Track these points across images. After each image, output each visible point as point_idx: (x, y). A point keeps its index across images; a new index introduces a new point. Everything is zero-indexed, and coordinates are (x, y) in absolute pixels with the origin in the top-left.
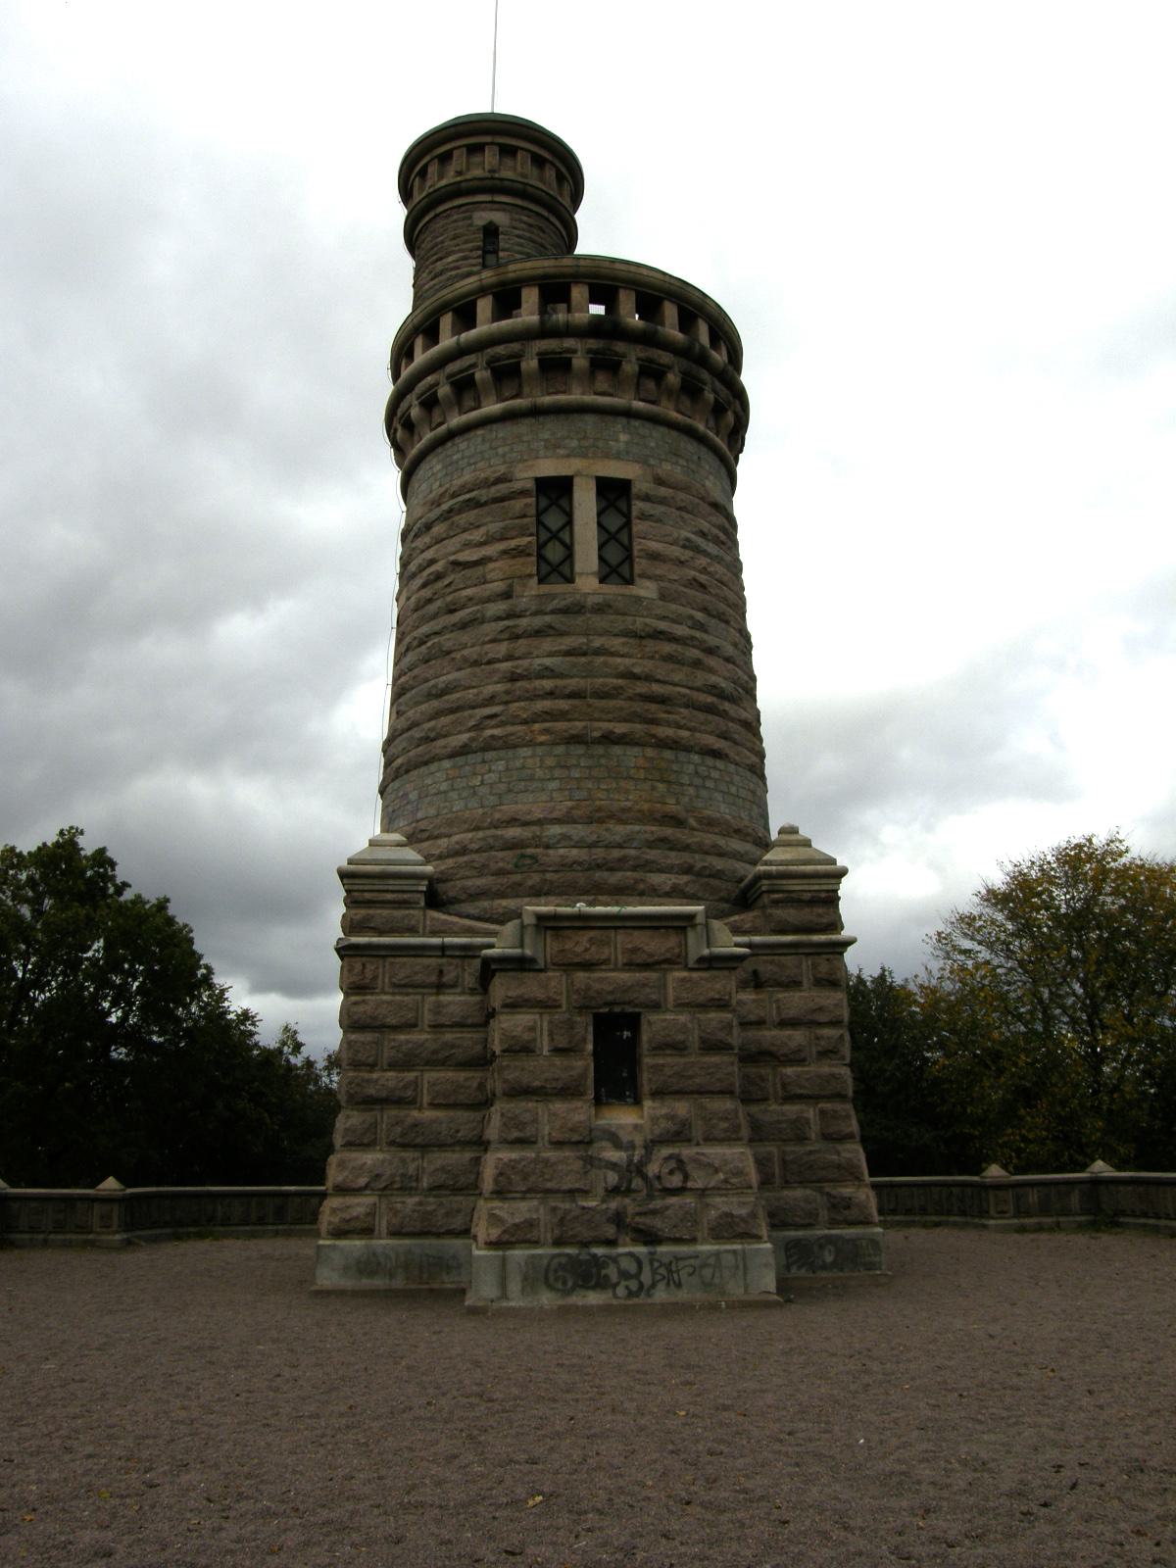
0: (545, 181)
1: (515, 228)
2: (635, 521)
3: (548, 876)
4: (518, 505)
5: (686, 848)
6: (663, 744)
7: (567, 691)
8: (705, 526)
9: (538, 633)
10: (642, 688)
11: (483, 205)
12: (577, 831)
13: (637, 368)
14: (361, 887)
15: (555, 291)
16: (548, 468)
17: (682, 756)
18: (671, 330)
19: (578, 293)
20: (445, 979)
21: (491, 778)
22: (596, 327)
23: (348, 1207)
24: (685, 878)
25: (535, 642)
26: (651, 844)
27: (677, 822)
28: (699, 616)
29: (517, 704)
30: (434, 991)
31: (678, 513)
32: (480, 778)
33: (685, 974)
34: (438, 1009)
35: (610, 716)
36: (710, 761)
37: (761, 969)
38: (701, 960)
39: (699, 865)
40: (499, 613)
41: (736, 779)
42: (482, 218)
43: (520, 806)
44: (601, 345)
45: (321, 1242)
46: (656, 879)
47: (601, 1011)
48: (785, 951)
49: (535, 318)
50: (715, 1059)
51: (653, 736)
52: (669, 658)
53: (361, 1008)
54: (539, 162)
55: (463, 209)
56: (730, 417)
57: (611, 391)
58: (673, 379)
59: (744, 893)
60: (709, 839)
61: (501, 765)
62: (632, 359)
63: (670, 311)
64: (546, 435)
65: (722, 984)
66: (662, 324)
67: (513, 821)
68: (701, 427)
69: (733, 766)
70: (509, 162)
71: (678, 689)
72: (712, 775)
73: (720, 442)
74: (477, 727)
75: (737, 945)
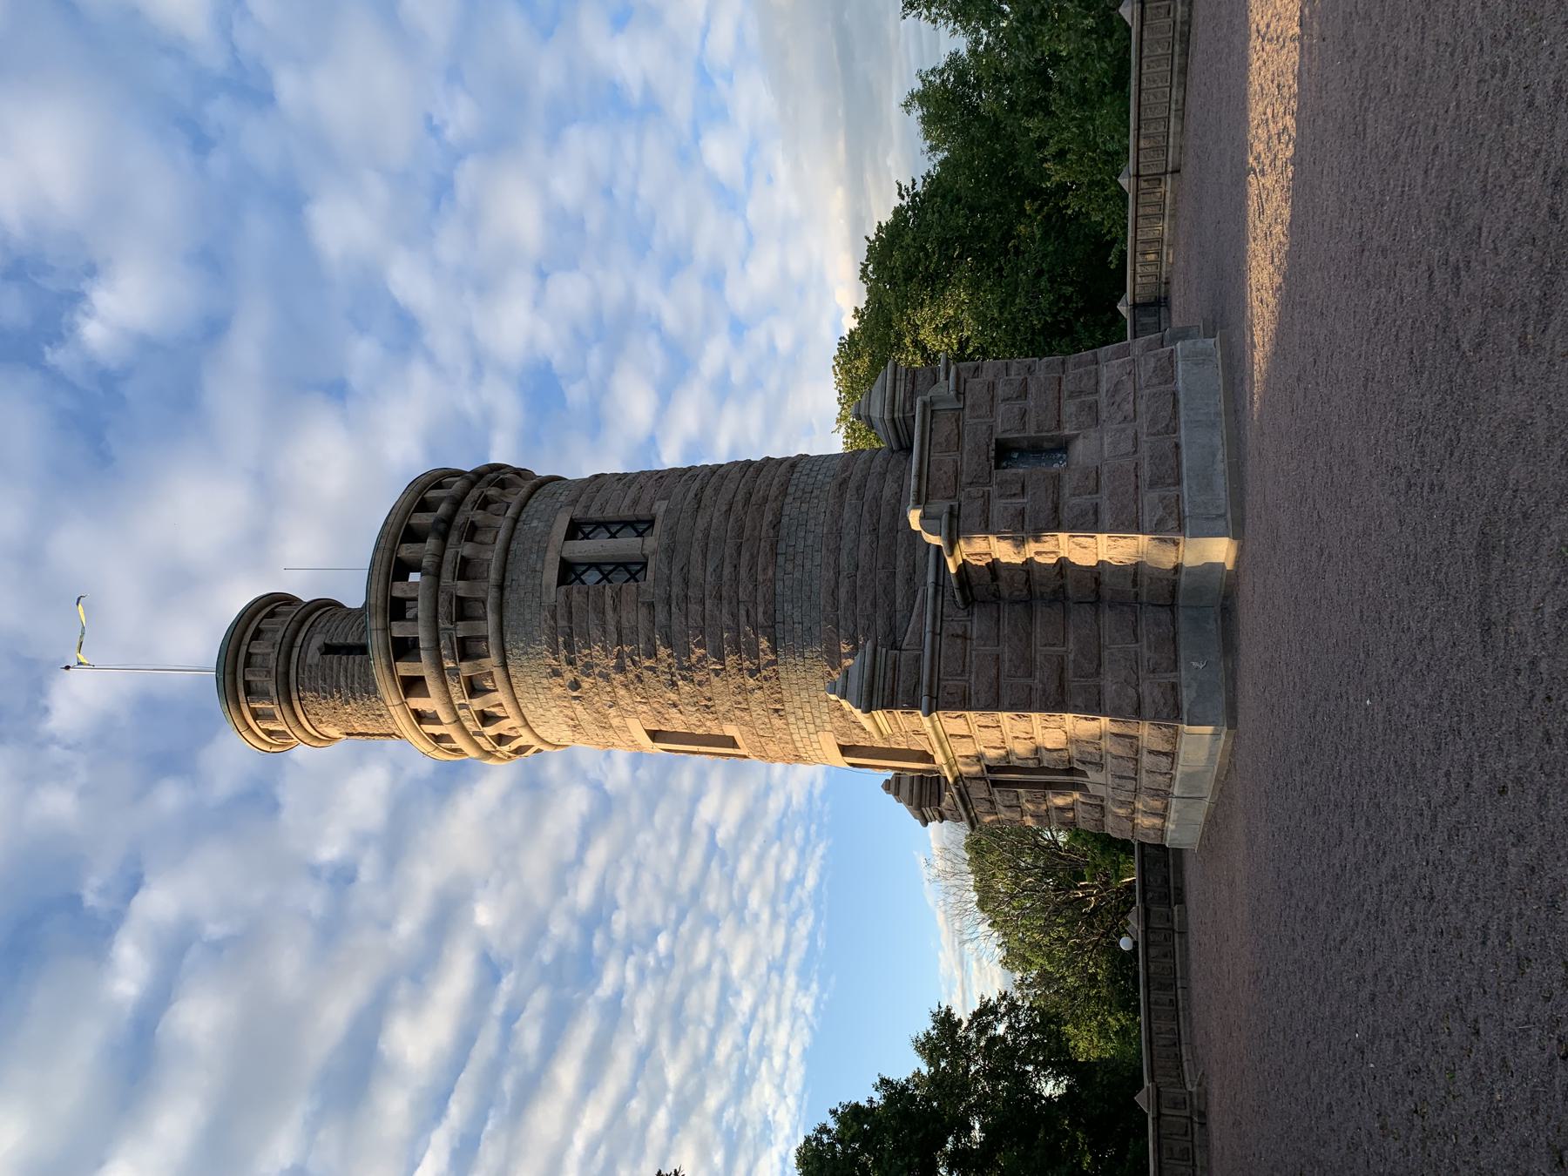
0: (278, 628)
3: (880, 565)
5: (865, 478)
9: (686, 582)
10: (738, 506)
11: (302, 655)
12: (847, 544)
14: (880, 698)
16: (551, 574)
19: (399, 590)
21: (797, 616)
26: (861, 498)
27: (843, 484)
29: (740, 595)
32: (796, 626)
33: (967, 411)
35: (758, 525)
39: (878, 469)
40: (665, 613)
42: (313, 656)
46: (887, 492)
50: (1033, 389)
51: (776, 497)
52: (717, 491)
54: (258, 634)
55: (300, 671)
57: (494, 532)
62: (468, 513)
63: (407, 551)
64: (523, 578)
67: (834, 593)
73: (514, 499)
75: (947, 378)
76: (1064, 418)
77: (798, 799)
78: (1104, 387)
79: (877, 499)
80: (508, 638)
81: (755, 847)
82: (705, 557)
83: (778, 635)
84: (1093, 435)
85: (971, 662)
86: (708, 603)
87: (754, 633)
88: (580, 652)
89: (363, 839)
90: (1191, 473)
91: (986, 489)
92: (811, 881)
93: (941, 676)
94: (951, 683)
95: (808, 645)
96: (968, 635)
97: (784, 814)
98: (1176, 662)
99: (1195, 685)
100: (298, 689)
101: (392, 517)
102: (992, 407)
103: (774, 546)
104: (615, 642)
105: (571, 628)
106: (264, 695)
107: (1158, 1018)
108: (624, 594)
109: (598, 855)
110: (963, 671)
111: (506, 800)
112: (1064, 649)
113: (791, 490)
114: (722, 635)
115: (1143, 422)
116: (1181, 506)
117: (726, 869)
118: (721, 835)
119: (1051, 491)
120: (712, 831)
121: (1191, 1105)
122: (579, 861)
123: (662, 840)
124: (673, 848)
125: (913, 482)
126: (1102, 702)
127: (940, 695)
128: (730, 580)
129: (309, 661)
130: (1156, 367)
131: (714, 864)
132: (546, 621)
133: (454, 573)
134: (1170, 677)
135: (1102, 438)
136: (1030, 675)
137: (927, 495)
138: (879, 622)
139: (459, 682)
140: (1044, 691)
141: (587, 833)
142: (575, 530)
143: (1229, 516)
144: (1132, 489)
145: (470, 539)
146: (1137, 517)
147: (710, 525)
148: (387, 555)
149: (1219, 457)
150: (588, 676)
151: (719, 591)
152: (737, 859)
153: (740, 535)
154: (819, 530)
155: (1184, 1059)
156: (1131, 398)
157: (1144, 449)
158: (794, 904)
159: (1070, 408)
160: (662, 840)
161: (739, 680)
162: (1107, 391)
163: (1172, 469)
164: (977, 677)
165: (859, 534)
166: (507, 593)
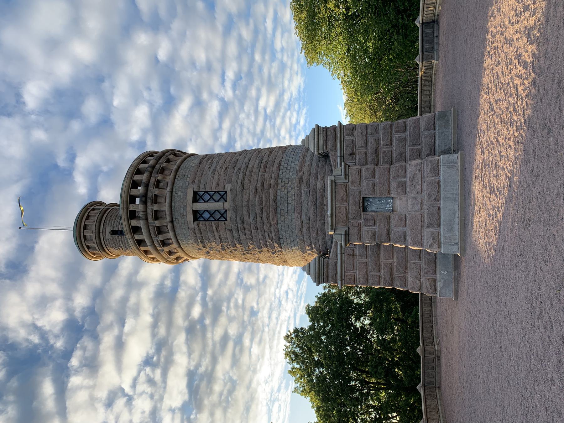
1: (111, 225)
2: (206, 190)
3: (318, 220)
4: (202, 227)
5: (309, 176)
6: (277, 184)
7: (261, 213)
8: (207, 167)
9: (243, 222)
10: (259, 189)
11: (104, 235)
12: (304, 210)
13: (157, 189)
14: (323, 279)
15: (133, 215)
16: (190, 217)
17: (280, 176)
18: (144, 177)
19: (132, 207)
20: (352, 254)
21: (288, 237)
22: (144, 202)
23: (427, 287)
24: (319, 176)
25: (245, 223)
26: (308, 188)
27: (301, 178)
28: (236, 170)
29: (265, 228)
30: (355, 256)
31: (203, 176)
33: (350, 183)
34: (361, 256)
36: (281, 167)
37: (348, 153)
38: (346, 178)
39: (315, 172)
41: (287, 158)
42: (108, 236)
43: (297, 228)
44: (150, 201)
45: (438, 296)
46: (319, 186)
47: (362, 210)
48: (342, 145)
49: (141, 221)
50: (378, 174)
51: (274, 186)
53: (361, 280)
55: (105, 241)
56: (171, 157)
57: (164, 197)
58: (160, 177)
59: (324, 156)
60: (306, 168)
61: (284, 233)
62: (153, 191)
65: (353, 169)
66: (142, 180)
67: (301, 230)
68: (175, 167)
69: (283, 159)
70: (89, 227)
71: (259, 177)
72: (286, 166)
73: (180, 159)
74: (272, 240)
75: (341, 166)
76: (391, 188)
77: (295, 93)
78: (408, 176)
79: (315, 189)
80: (179, 238)
81: (281, 114)
82: (249, 213)
83: (281, 243)
84: (403, 198)
85: (356, 265)
86: (252, 231)
87: (272, 242)
88: (207, 244)
89: (145, 131)
90: (445, 223)
91: (359, 221)
92: (302, 122)
93: (345, 270)
94: (349, 273)
95: (293, 246)
96: (355, 254)
97: (290, 100)
98: (435, 271)
99: (442, 281)
100: (106, 247)
101: (123, 193)
102: (360, 182)
103: (275, 210)
104: (220, 242)
105: (202, 237)
106: (95, 249)
107: (425, 306)
108: (220, 226)
109: (226, 124)
110: (353, 269)
111: (191, 109)
112: (393, 261)
113: (280, 181)
114: (260, 242)
115: (425, 194)
116: (440, 237)
117: (272, 123)
118: (268, 111)
119: (386, 225)
120: (265, 110)
121: (435, 354)
122: (220, 128)
123: (248, 116)
124: (253, 119)
125: (329, 219)
126: (407, 284)
127: (345, 278)
128: (260, 223)
129: (107, 238)
130: (431, 169)
131: (268, 122)
132: (192, 234)
133: (153, 218)
134: (433, 276)
135: (407, 201)
136: (380, 271)
137: (335, 224)
138: (320, 240)
139: (165, 253)
140: (385, 279)
141: (221, 115)
142: (196, 197)
143: (459, 244)
144: (420, 228)
145: (156, 202)
146: (422, 240)
147: (249, 199)
148: (125, 211)
149: (457, 215)
150: (212, 250)
151: (256, 227)
152: (275, 119)
153: (262, 204)
154: (293, 203)
155: (434, 323)
156: (420, 183)
157: (425, 208)
158: (297, 132)
159: (394, 184)
160: (248, 116)
161: (268, 254)
162: (410, 178)
163: (437, 220)
164: (359, 272)
165: (309, 206)
166: (175, 223)
